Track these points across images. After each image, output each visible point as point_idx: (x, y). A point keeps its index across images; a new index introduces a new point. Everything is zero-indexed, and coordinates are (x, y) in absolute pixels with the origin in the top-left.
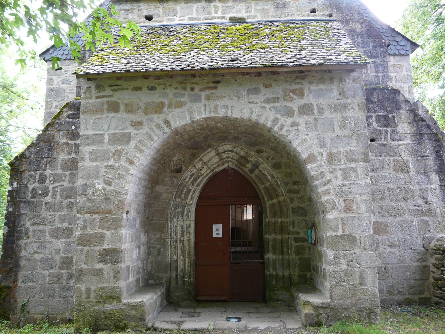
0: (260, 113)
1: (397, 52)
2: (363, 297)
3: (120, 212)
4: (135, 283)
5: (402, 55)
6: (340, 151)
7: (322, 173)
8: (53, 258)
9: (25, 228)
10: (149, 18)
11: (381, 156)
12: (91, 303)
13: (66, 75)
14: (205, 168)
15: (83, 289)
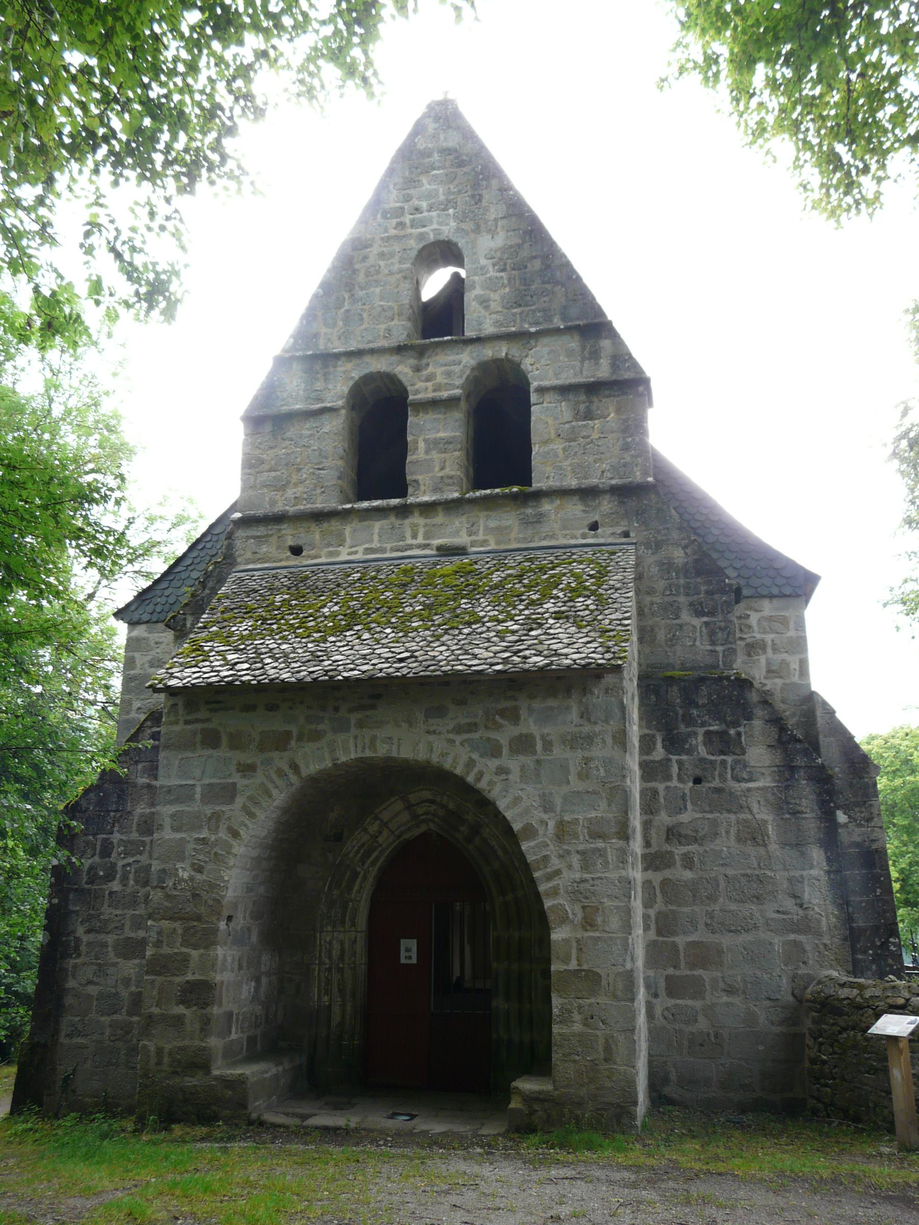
0: (445, 751)
1: (775, 591)
2: (608, 1084)
3: (214, 919)
4: (245, 1044)
5: (786, 596)
6: (577, 820)
7: (546, 858)
8: (118, 993)
9: (75, 937)
10: (296, 551)
11: (711, 812)
12: (163, 1074)
13: (158, 650)
14: (386, 833)
15: (153, 1049)
